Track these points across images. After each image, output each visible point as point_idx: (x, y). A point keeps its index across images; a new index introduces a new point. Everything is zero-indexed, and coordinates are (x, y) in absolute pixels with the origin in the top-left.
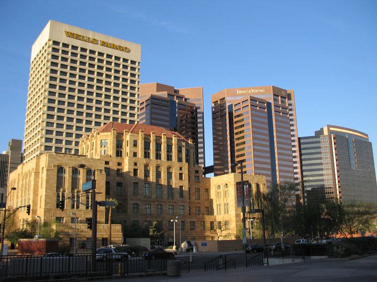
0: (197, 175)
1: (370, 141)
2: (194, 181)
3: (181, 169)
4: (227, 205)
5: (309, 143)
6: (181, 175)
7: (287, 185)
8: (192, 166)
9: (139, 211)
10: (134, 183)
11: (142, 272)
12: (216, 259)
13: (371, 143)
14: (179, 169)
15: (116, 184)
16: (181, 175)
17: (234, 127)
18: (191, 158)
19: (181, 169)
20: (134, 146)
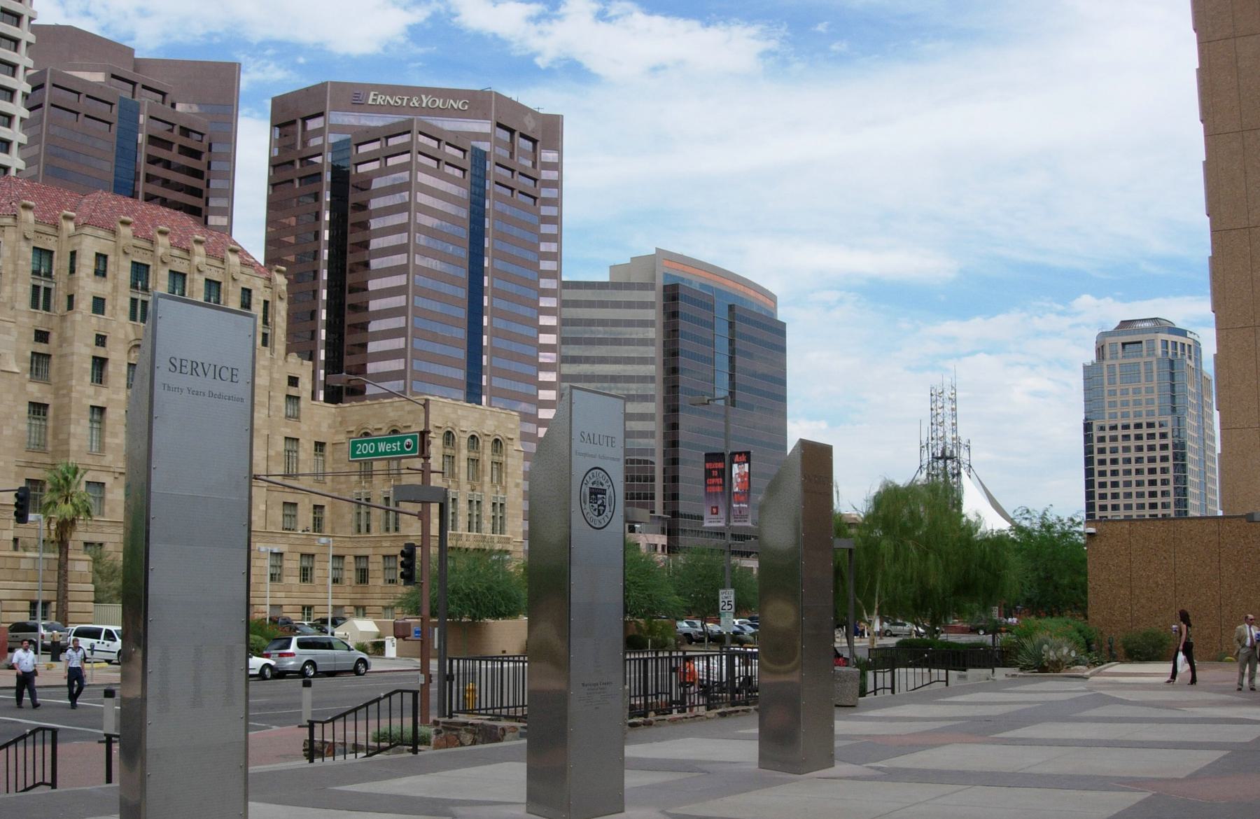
0: (293, 391)
1: (780, 318)
2: (283, 415)
3: (101, 340)
4: (499, 506)
5: (591, 304)
6: (100, 364)
7: (1059, 527)
8: (280, 363)
9: (107, 509)
10: (93, 407)
11: (635, 660)
12: (389, 695)
13: (784, 325)
14: (93, 341)
15: (26, 408)
16: (100, 364)
17: (350, 221)
18: (60, 285)
19: (101, 340)
20: (96, 273)
